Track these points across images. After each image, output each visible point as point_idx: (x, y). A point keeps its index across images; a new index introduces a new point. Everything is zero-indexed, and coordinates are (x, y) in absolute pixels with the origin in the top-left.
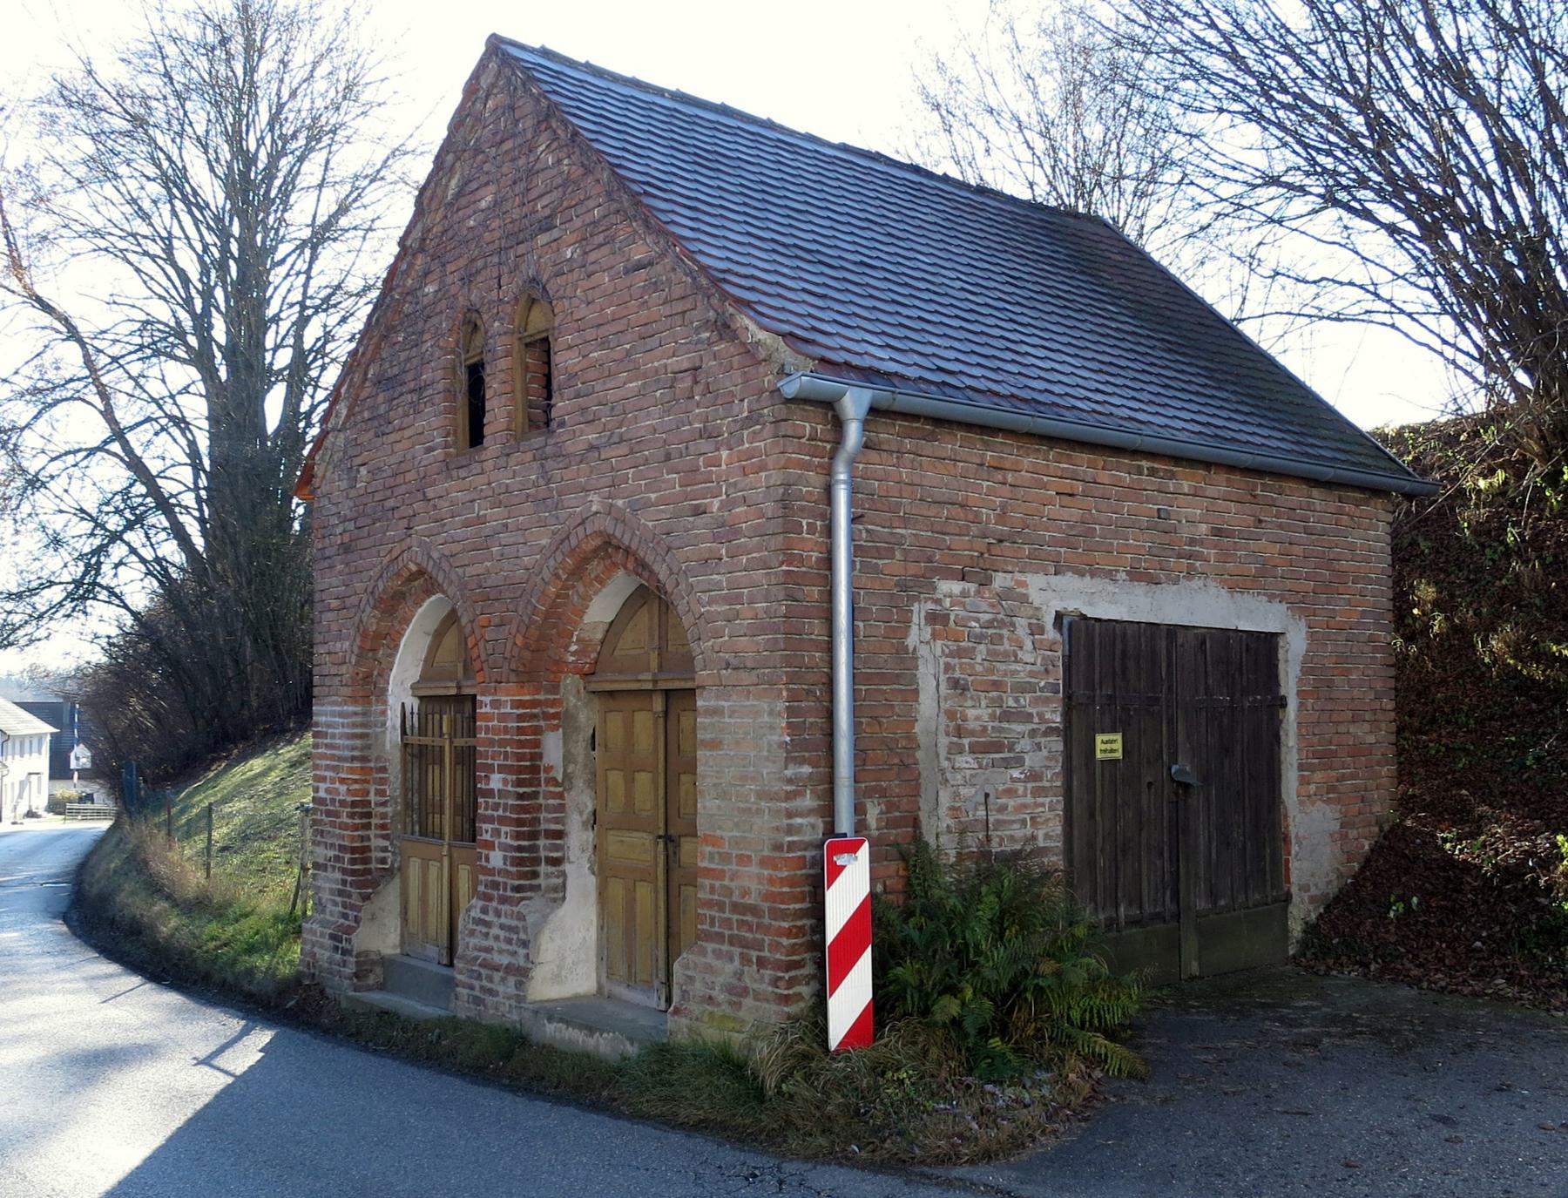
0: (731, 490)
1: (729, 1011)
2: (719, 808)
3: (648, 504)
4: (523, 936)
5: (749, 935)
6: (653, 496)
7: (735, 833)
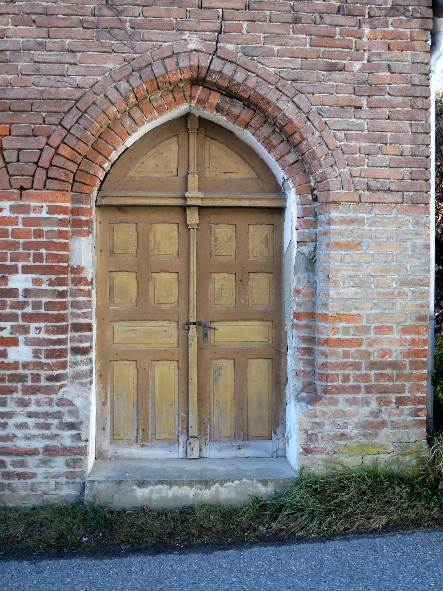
0: (374, 58)
1: (364, 441)
2: (356, 293)
3: (269, 54)
4: (68, 419)
5: (390, 384)
6: (276, 48)
7: (373, 311)
